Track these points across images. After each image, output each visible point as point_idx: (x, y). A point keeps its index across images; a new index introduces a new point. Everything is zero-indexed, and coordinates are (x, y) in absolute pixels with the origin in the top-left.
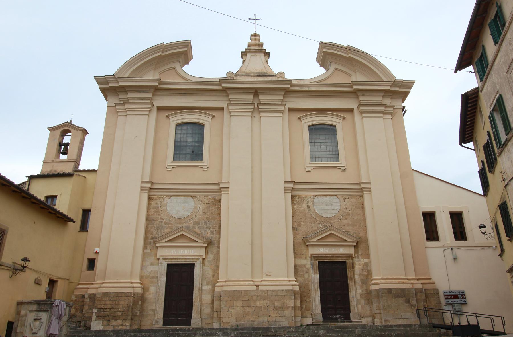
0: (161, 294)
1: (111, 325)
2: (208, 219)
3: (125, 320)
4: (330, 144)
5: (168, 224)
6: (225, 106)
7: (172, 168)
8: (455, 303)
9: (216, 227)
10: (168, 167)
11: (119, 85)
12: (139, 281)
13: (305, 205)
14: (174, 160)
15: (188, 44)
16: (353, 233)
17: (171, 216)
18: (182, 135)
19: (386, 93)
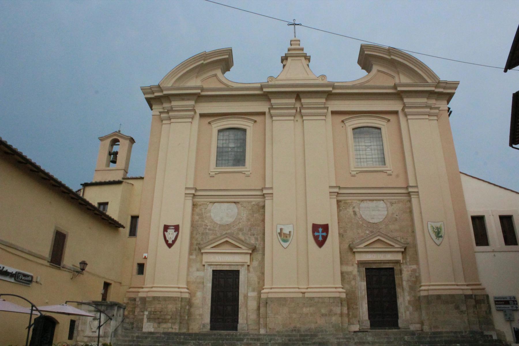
4: (376, 147)
6: (267, 110)
9: (260, 233)
11: (164, 94)
12: (186, 286)
13: (350, 210)
14: (216, 166)
15: (229, 52)
16: (401, 238)
17: (215, 223)
19: (430, 94)
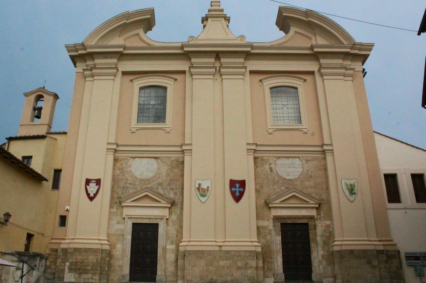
0: (127, 252)
1: (82, 277)
2: (171, 180)
3: (94, 274)
5: (133, 185)
6: (187, 69)
7: (136, 130)
8: (417, 264)
9: (179, 188)
10: (133, 130)
11: (87, 52)
13: (267, 167)
14: (137, 122)
15: (152, 12)
17: (136, 177)
18: (145, 99)
19: (346, 55)
